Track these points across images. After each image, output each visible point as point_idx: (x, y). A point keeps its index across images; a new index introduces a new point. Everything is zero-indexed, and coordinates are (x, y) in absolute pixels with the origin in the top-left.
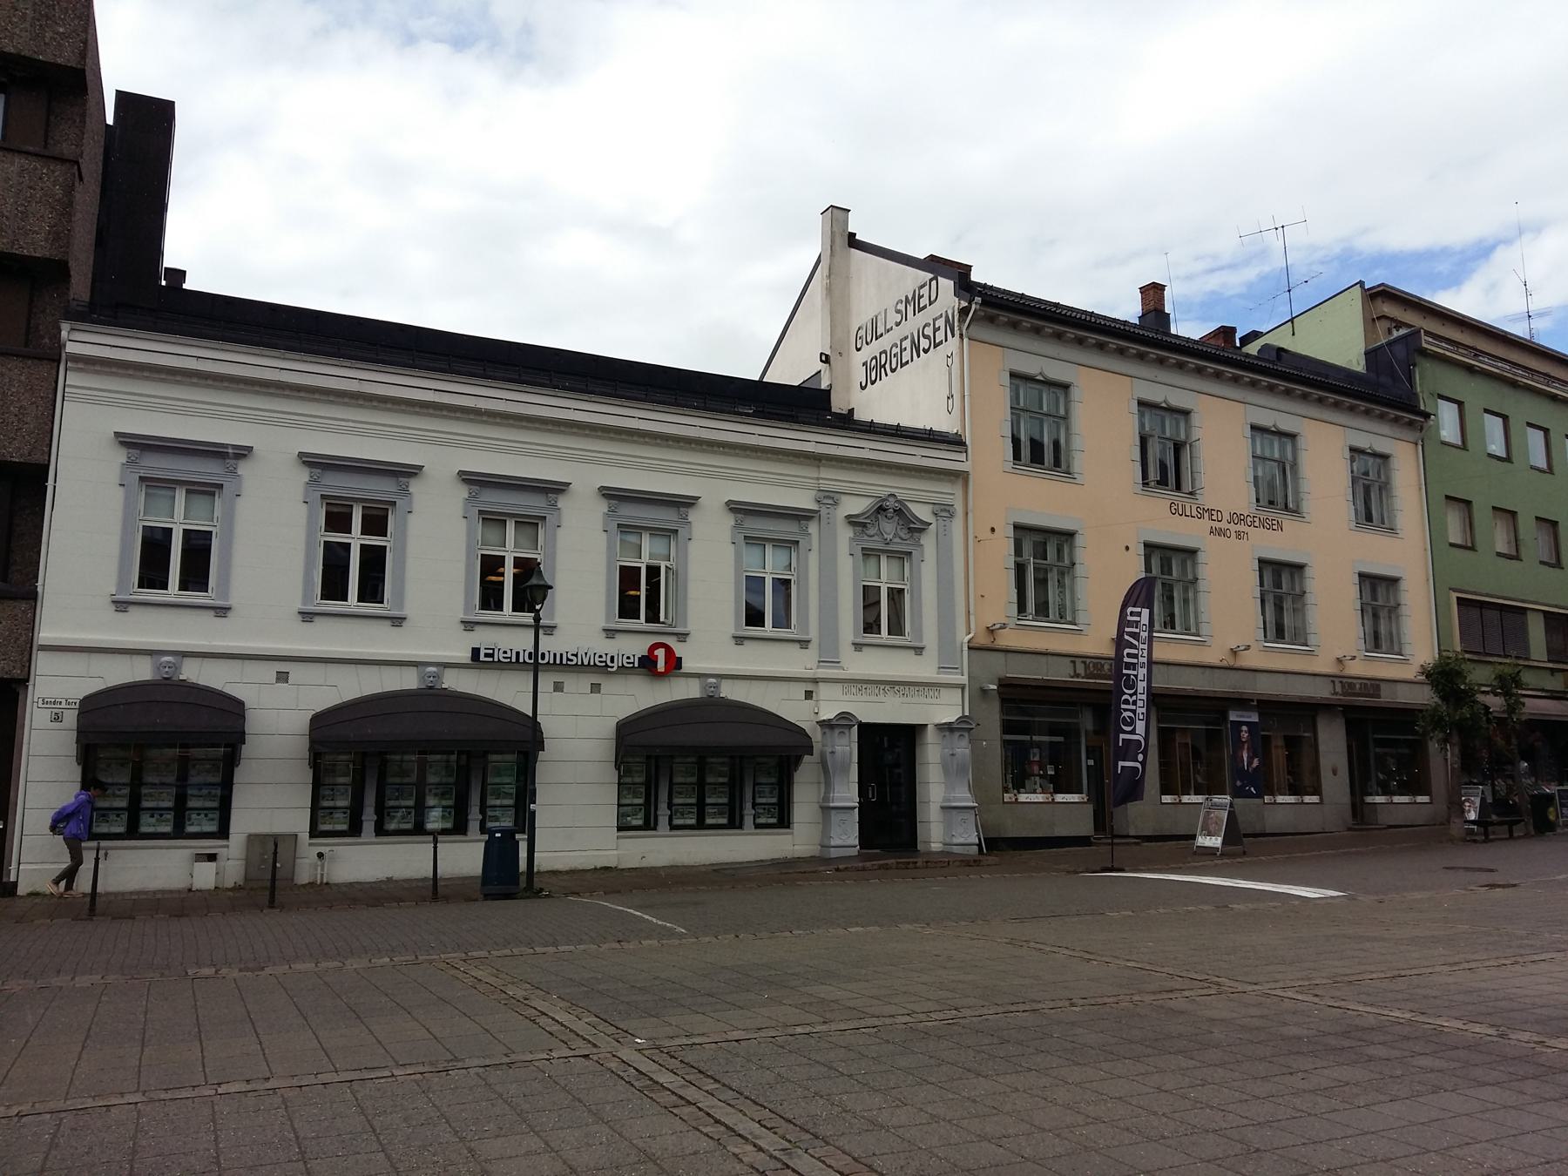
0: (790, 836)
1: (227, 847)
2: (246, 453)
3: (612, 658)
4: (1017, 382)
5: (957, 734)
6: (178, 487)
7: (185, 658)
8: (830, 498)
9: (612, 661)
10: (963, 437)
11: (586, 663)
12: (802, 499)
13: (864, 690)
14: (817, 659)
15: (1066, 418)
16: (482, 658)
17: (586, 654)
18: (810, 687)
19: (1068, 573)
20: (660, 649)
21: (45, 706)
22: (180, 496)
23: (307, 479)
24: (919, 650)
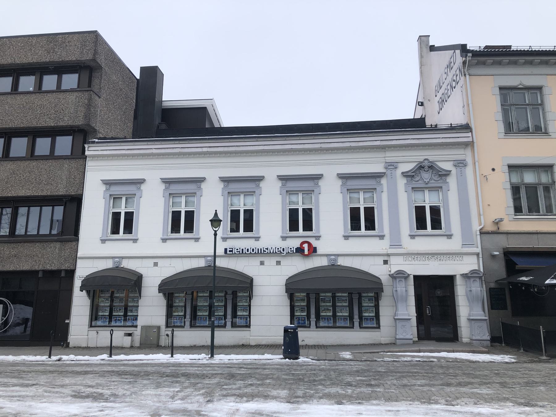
0: (379, 333)
1: (137, 331)
2: (383, 175)
3: (283, 249)
4: (504, 92)
5: (472, 280)
6: (299, 193)
7: (339, 257)
8: (392, 166)
9: (283, 250)
10: (470, 125)
11: (272, 252)
12: (378, 168)
13: (416, 259)
14: (462, 244)
15: (542, 104)
16: (228, 252)
17: (272, 248)
18: (386, 258)
19: (552, 187)
20: (306, 244)
21: (80, 278)
22: (242, 196)
23: (341, 184)
24: (450, 236)
